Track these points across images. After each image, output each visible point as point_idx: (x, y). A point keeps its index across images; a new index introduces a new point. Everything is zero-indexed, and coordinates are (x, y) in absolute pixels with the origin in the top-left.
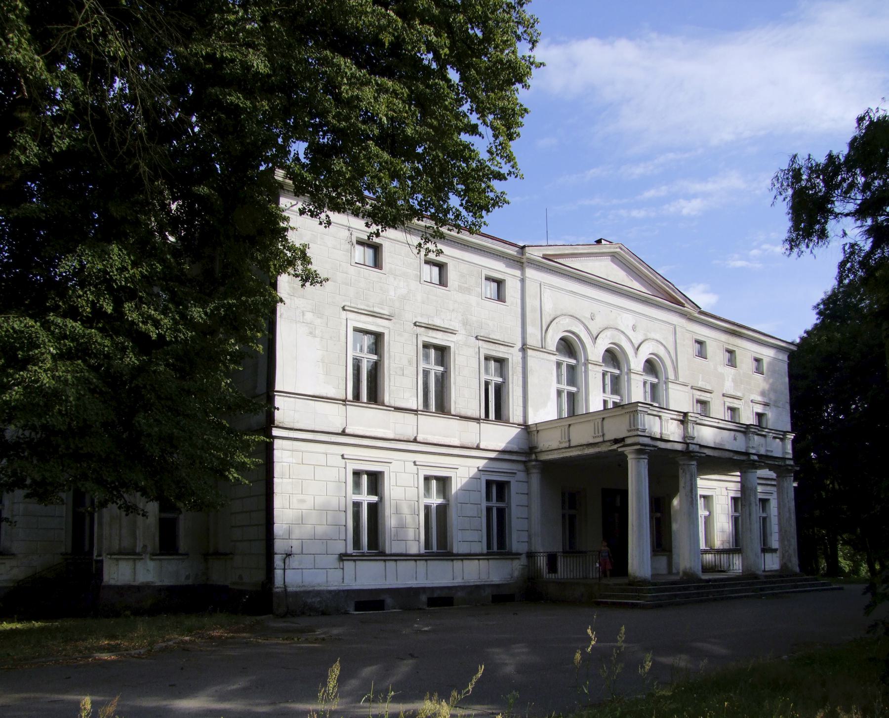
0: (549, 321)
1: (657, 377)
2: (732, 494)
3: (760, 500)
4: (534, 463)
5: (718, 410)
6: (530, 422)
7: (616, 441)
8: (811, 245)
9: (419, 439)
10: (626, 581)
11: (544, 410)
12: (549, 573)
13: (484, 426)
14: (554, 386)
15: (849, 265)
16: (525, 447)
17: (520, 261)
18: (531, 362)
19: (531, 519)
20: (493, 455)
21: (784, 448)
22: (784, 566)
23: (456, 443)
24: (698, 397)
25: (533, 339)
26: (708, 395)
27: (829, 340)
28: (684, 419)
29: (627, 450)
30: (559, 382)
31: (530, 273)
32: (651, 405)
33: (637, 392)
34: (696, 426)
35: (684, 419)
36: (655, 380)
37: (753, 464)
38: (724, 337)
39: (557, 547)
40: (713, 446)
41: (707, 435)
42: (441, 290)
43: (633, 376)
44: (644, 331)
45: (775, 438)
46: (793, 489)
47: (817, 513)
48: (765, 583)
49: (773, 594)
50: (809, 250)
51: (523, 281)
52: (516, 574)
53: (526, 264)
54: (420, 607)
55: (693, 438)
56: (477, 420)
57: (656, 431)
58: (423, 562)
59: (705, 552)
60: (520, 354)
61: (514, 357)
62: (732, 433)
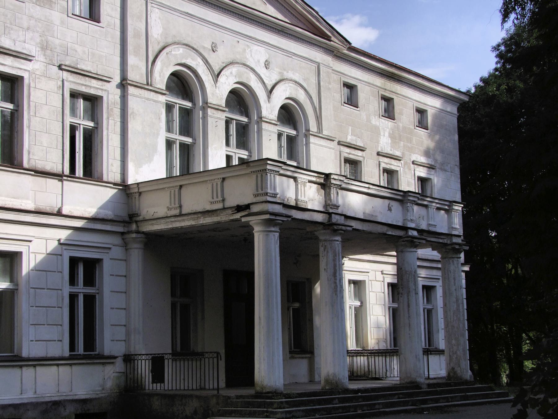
0: (157, 48)
1: (295, 128)
2: (390, 279)
3: (424, 287)
4: (134, 235)
5: (371, 173)
6: (130, 181)
7: (239, 208)
10: (251, 392)
11: (150, 166)
13: (69, 185)
14: (163, 136)
16: (123, 214)
18: (132, 103)
20: (79, 224)
21: (450, 222)
23: (30, 206)
24: (346, 155)
25: (136, 73)
26: (360, 153)
27: (510, 90)
28: (325, 182)
30: (169, 129)
32: (284, 163)
33: (270, 147)
34: (340, 192)
35: (325, 182)
36: (293, 132)
37: (412, 242)
38: (379, 81)
39: (164, 347)
41: (355, 202)
43: (264, 126)
45: (438, 209)
48: (428, 393)
52: (109, 384)
55: (337, 207)
56: (59, 176)
59: (357, 354)
60: (118, 91)
61: (111, 95)
62: (387, 201)
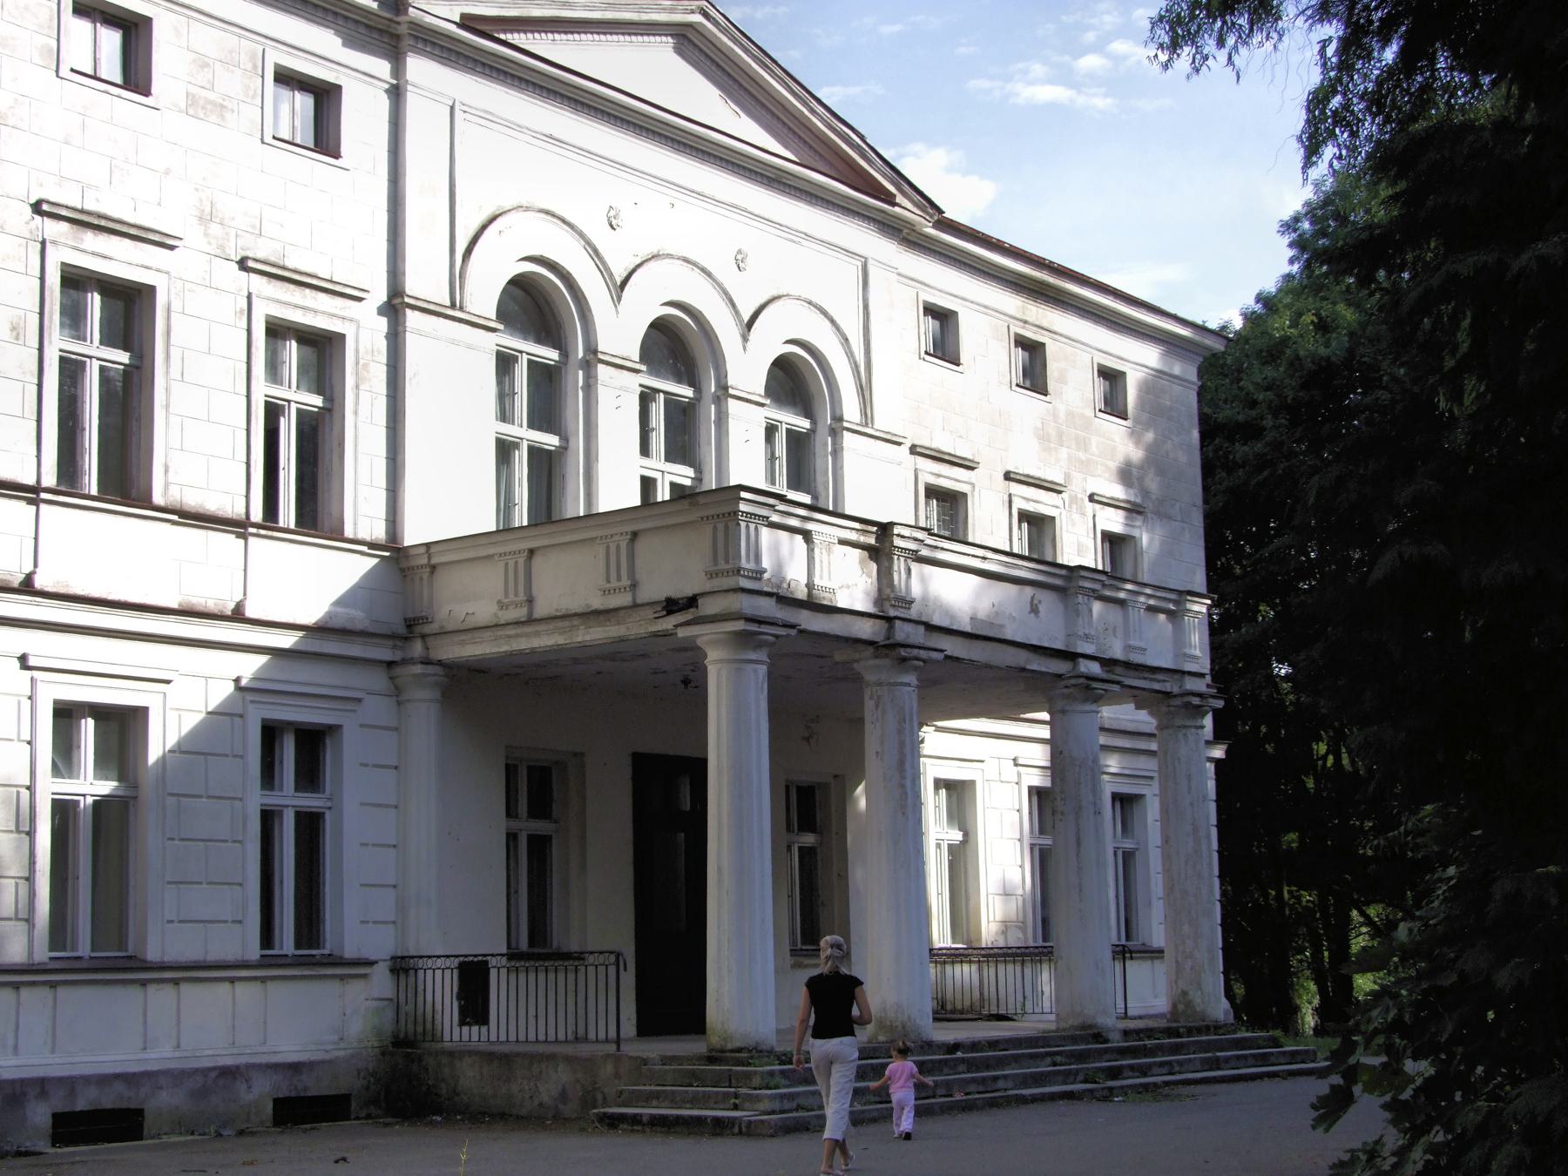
1: (808, 413)
2: (1036, 779)
3: (1116, 797)
4: (418, 669)
5: (991, 522)
7: (671, 606)
8: (1231, 41)
9: (40, 582)
12: (462, 1023)
15: (1336, 101)
17: (390, 34)
19: (418, 860)
20: (286, 640)
21: (1179, 639)
22: (1181, 1003)
24: (933, 480)
25: (426, 278)
27: (1323, 326)
28: (880, 543)
29: (704, 635)
30: (504, 415)
31: (419, 68)
34: (915, 567)
35: (880, 543)
36: (803, 424)
38: (1012, 303)
39: (486, 935)
40: (968, 629)
41: (951, 592)
42: (126, 105)
44: (773, 269)
46: (1211, 767)
47: (1291, 838)
49: (1146, 1086)
50: (1222, 55)
51: (396, 94)
53: (408, 41)
54: (28, 1145)
55: (908, 602)
56: (238, 526)
57: (796, 575)
58: (45, 992)
59: (954, 957)
